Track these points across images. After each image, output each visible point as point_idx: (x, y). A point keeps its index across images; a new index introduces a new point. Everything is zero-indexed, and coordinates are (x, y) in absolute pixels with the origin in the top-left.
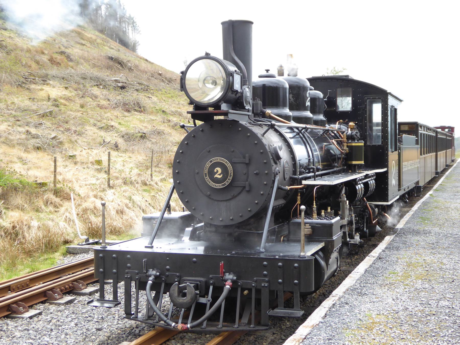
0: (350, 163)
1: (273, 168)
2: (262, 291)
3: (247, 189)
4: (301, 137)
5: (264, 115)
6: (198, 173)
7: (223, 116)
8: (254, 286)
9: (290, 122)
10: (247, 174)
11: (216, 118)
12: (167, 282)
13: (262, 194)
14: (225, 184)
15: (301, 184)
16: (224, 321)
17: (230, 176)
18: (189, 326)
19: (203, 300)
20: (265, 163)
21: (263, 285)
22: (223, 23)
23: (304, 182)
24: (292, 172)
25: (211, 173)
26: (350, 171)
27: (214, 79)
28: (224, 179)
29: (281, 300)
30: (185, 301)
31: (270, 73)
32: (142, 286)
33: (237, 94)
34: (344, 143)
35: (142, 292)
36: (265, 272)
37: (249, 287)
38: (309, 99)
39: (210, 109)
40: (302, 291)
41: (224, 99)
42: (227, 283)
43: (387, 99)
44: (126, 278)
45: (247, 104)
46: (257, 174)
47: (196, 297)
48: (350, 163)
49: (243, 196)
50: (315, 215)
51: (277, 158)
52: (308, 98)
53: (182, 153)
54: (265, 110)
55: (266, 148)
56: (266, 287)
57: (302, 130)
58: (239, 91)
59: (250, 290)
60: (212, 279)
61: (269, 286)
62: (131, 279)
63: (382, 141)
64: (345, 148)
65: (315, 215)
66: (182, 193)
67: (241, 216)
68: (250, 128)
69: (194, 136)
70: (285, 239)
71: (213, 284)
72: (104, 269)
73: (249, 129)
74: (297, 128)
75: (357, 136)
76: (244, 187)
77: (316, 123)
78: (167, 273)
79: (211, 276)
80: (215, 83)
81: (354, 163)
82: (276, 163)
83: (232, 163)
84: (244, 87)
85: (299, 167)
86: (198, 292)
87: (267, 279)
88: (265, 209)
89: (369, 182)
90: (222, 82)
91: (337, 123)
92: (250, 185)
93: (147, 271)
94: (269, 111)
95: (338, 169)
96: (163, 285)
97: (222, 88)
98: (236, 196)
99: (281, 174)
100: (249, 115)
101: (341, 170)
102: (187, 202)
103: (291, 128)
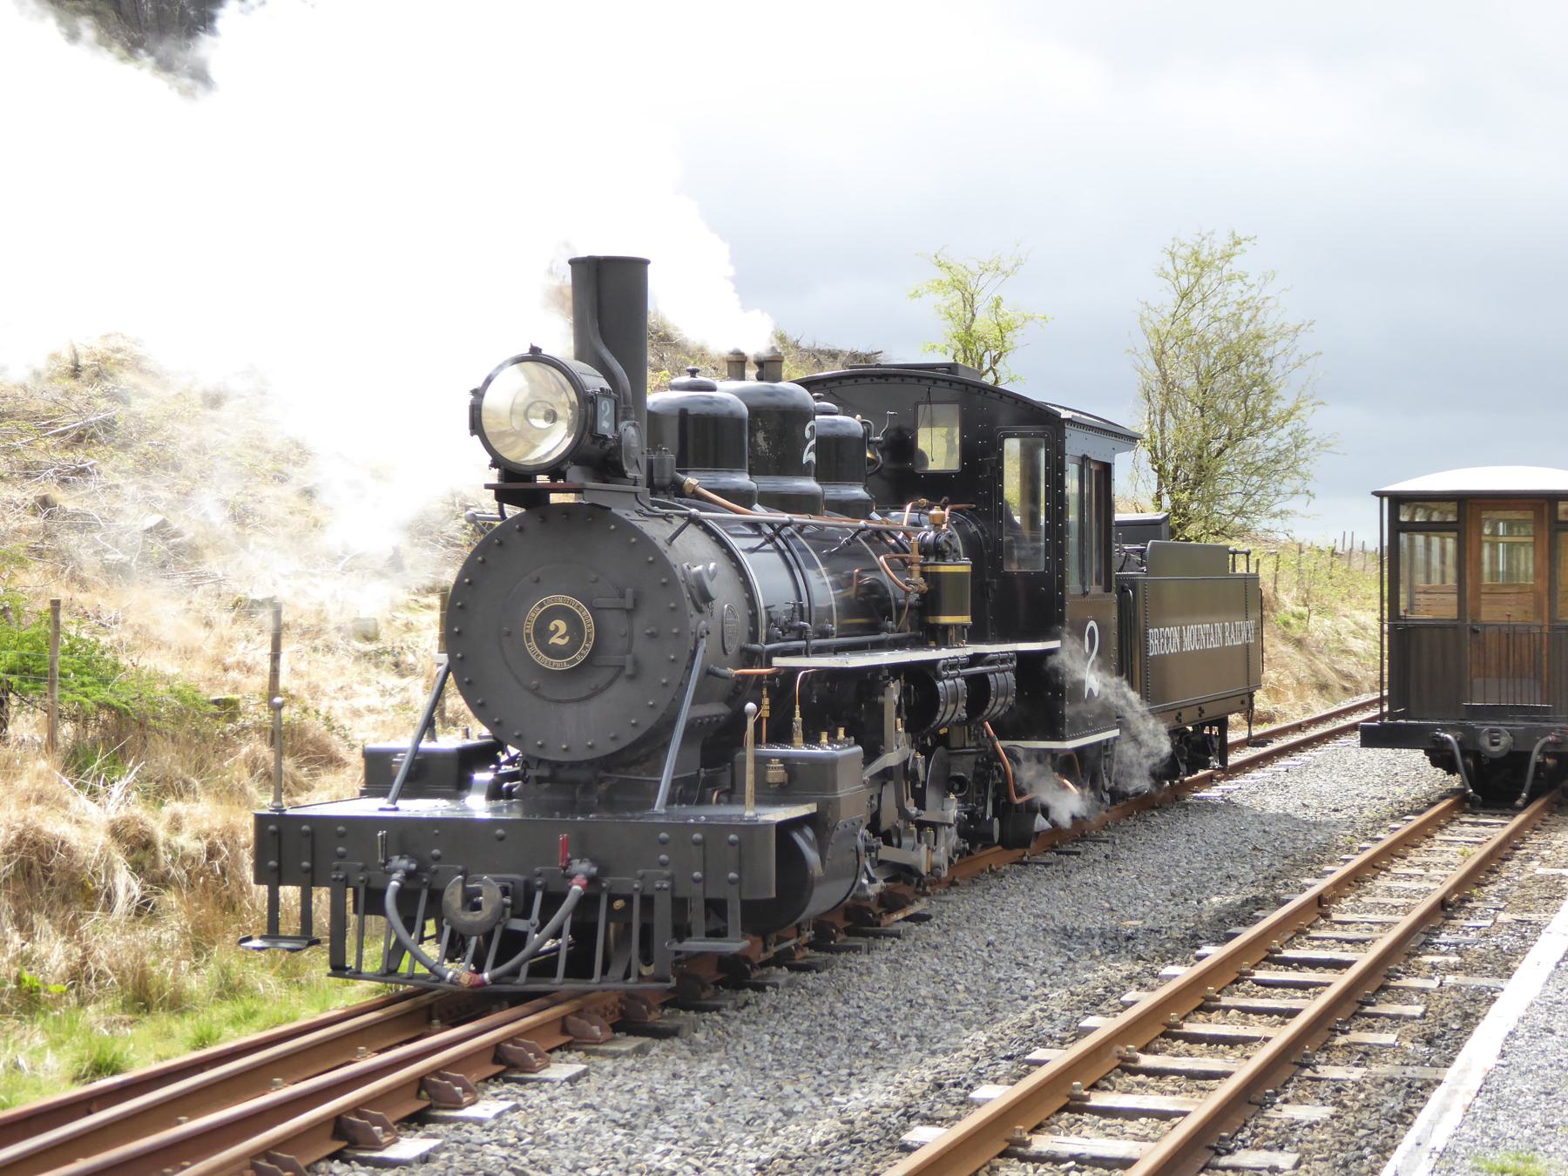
0: (931, 620)
1: (692, 622)
2: (657, 900)
3: (629, 670)
4: (778, 548)
5: (678, 490)
6: (509, 634)
7: (573, 495)
8: (637, 890)
9: (750, 508)
10: (629, 636)
11: (555, 498)
12: (434, 887)
13: (665, 685)
14: (575, 660)
15: (769, 665)
16: (567, 974)
17: (589, 640)
18: (486, 976)
19: (518, 925)
20: (673, 609)
21: (658, 885)
22: (576, 263)
23: (778, 662)
24: (746, 635)
25: (542, 632)
26: (933, 644)
27: (550, 407)
28: (573, 647)
29: (697, 918)
30: (478, 919)
31: (699, 378)
32: (372, 902)
33: (604, 443)
34: (912, 564)
35: (372, 920)
36: (663, 857)
37: (626, 891)
38: (813, 442)
39: (542, 479)
40: (746, 897)
41: (574, 455)
42: (574, 881)
43: (1063, 438)
44: (335, 880)
45: (630, 468)
46: (652, 636)
47: (503, 914)
48: (931, 620)
49: (620, 689)
50: (798, 738)
51: (703, 597)
52: (807, 441)
53: (469, 583)
54: (683, 477)
55: (674, 574)
56: (666, 889)
57: (781, 528)
58: (610, 437)
59: (628, 899)
60: (539, 875)
61: (673, 888)
62: (346, 882)
63: (1047, 561)
64: (917, 578)
65: (798, 738)
66: (469, 683)
67: (614, 739)
68: (637, 524)
69: (501, 544)
70: (724, 798)
71: (544, 888)
72: (279, 862)
73: (634, 527)
74: (771, 524)
75: (950, 546)
76: (622, 668)
77: (844, 507)
78: (434, 867)
79: (537, 869)
80: (552, 416)
81: (945, 620)
82: (700, 611)
83: (593, 610)
84: (622, 425)
85: (764, 623)
86: (508, 900)
87: (667, 872)
88: (669, 723)
89: (991, 677)
90: (569, 411)
91: (909, 507)
92: (636, 663)
93: (387, 861)
94: (691, 480)
95: (892, 636)
96: (424, 894)
97: (569, 429)
98: (602, 690)
99: (715, 636)
100: (636, 494)
101: (910, 637)
102: (482, 705)
103: (755, 525)
